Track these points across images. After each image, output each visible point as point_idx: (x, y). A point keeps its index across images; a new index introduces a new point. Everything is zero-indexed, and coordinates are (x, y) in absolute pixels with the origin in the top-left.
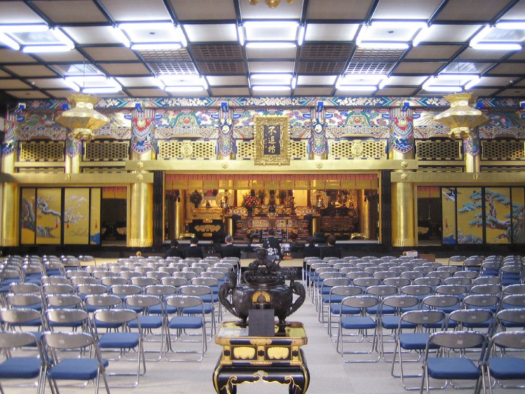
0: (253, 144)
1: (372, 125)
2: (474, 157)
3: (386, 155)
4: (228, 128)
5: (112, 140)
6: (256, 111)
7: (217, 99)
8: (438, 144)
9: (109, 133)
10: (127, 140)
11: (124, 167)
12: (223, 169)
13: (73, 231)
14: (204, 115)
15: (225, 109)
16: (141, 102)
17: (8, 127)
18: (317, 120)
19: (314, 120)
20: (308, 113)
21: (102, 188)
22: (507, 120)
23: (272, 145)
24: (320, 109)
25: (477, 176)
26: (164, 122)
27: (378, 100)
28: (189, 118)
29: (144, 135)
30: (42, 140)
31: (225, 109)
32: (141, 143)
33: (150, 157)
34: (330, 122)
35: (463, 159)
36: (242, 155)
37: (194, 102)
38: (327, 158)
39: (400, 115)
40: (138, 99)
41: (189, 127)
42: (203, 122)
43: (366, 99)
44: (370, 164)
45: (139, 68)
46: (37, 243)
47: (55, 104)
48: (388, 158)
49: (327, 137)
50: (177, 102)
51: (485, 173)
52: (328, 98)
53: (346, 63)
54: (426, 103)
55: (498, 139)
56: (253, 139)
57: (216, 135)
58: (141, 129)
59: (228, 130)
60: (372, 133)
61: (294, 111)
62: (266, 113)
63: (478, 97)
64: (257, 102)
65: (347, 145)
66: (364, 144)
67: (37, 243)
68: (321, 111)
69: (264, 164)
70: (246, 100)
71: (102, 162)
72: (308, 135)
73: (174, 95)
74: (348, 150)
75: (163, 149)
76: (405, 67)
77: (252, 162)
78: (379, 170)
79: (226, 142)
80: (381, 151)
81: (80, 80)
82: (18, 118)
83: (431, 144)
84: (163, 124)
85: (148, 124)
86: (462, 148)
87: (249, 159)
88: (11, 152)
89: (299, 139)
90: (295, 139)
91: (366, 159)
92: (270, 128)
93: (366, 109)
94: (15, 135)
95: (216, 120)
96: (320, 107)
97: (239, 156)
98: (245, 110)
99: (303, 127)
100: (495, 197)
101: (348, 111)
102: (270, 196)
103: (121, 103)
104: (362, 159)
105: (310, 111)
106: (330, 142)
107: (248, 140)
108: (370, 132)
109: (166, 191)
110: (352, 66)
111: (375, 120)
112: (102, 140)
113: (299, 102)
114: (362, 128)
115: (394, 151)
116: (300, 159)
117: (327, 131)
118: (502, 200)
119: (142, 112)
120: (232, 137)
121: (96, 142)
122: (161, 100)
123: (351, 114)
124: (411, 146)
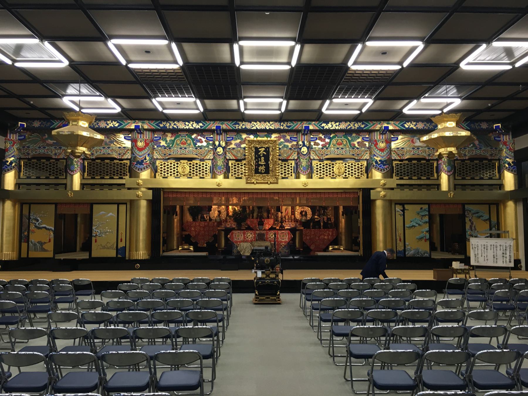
0: (245, 164)
1: (353, 147)
2: (449, 176)
3: (365, 175)
4: (221, 149)
5: (113, 159)
6: (247, 134)
7: (212, 122)
8: (414, 164)
9: (110, 152)
10: (127, 159)
11: (124, 184)
12: (218, 187)
13: (101, 245)
14: (199, 137)
15: (219, 132)
16: (140, 124)
17: (8, 145)
18: (303, 142)
19: (301, 143)
20: (295, 136)
21: (56, 204)
22: (480, 142)
23: (262, 165)
24: (306, 132)
25: (452, 195)
26: (163, 143)
27: (359, 124)
28: (185, 139)
29: (144, 154)
30: (43, 158)
31: (219, 132)
32: (141, 163)
33: (149, 176)
34: (314, 145)
35: (439, 176)
36: (235, 174)
37: (190, 125)
38: (312, 178)
39: (380, 138)
40: (137, 121)
41: (185, 148)
42: (199, 144)
43: (349, 123)
44: (351, 183)
45: (137, 89)
46: (30, 256)
47: (56, 124)
48: (367, 177)
49: (312, 158)
50: (175, 124)
51: (459, 191)
52: (314, 123)
53: (335, 86)
54: (404, 127)
55: (471, 159)
56: (244, 159)
57: (211, 156)
58: (140, 150)
59: (222, 151)
60: (353, 155)
61: (282, 134)
62: (256, 136)
63: (464, 117)
64: (248, 126)
65: (330, 166)
66: (346, 164)
67: (30, 256)
68: (307, 134)
69: (255, 182)
70: (239, 124)
71: (103, 180)
72: (295, 156)
73: (172, 118)
74: (331, 170)
75: (161, 168)
76: (391, 90)
77: (243, 181)
78: (360, 189)
79: (220, 162)
80: (361, 171)
81: (78, 98)
82: (19, 136)
83: (408, 164)
84: (161, 145)
85: (147, 145)
86: (437, 167)
87: (241, 178)
88: (11, 169)
89: (286, 160)
90: (283, 160)
91: (347, 178)
92: (260, 150)
93: (347, 132)
94: (16, 153)
95: (211, 142)
96: (307, 130)
97: (232, 175)
98: (238, 133)
99: (290, 149)
100: (474, 214)
101: (331, 134)
102: (255, 210)
103: (121, 124)
104: (344, 178)
105: (297, 135)
106: (314, 163)
107: (240, 160)
108: (351, 153)
109: (164, 206)
110: (339, 93)
111: (356, 143)
112: (103, 159)
113: (287, 126)
114: (344, 150)
115: (373, 170)
116: (287, 178)
117: (312, 153)
118: (482, 216)
119: (141, 133)
120: (225, 157)
121: (97, 161)
122: (159, 123)
123: (334, 137)
124: (389, 167)
